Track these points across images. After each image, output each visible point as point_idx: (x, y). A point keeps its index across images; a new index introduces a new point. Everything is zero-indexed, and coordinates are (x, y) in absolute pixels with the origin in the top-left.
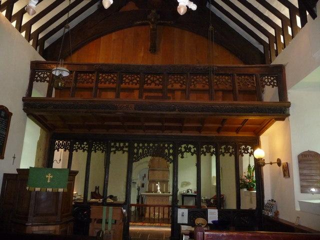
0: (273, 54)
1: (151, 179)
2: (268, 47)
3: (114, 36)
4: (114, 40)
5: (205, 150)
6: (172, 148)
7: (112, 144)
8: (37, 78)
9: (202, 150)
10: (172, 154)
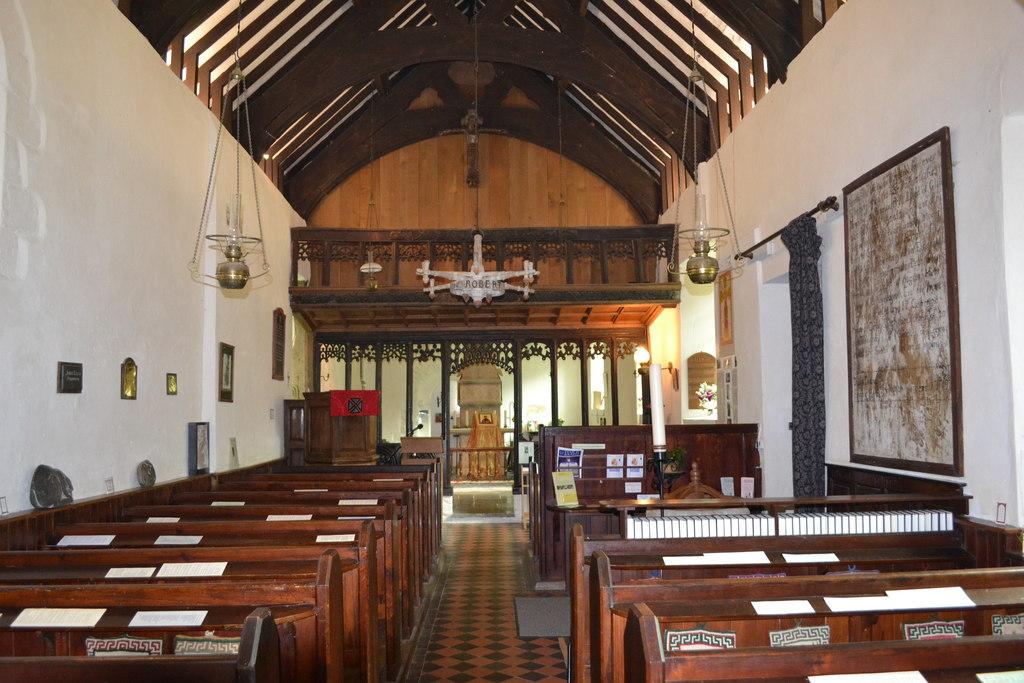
0: (724, 123)
2: (715, 107)
3: (402, 155)
4: (403, 163)
5: (564, 351)
6: (512, 350)
7: (415, 347)
9: (559, 350)
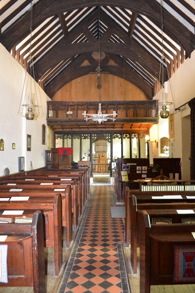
1: (97, 150)
5: (125, 136)
6: (110, 136)
8: (50, 109)
9: (123, 136)
10: (110, 139)
